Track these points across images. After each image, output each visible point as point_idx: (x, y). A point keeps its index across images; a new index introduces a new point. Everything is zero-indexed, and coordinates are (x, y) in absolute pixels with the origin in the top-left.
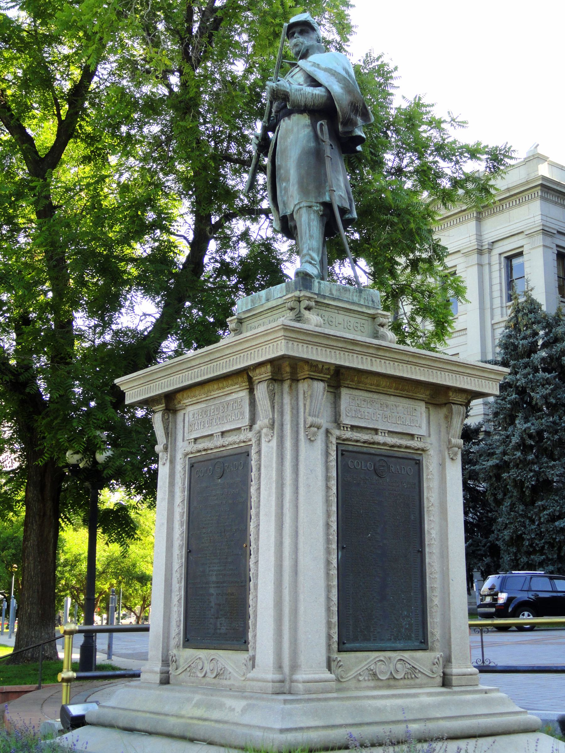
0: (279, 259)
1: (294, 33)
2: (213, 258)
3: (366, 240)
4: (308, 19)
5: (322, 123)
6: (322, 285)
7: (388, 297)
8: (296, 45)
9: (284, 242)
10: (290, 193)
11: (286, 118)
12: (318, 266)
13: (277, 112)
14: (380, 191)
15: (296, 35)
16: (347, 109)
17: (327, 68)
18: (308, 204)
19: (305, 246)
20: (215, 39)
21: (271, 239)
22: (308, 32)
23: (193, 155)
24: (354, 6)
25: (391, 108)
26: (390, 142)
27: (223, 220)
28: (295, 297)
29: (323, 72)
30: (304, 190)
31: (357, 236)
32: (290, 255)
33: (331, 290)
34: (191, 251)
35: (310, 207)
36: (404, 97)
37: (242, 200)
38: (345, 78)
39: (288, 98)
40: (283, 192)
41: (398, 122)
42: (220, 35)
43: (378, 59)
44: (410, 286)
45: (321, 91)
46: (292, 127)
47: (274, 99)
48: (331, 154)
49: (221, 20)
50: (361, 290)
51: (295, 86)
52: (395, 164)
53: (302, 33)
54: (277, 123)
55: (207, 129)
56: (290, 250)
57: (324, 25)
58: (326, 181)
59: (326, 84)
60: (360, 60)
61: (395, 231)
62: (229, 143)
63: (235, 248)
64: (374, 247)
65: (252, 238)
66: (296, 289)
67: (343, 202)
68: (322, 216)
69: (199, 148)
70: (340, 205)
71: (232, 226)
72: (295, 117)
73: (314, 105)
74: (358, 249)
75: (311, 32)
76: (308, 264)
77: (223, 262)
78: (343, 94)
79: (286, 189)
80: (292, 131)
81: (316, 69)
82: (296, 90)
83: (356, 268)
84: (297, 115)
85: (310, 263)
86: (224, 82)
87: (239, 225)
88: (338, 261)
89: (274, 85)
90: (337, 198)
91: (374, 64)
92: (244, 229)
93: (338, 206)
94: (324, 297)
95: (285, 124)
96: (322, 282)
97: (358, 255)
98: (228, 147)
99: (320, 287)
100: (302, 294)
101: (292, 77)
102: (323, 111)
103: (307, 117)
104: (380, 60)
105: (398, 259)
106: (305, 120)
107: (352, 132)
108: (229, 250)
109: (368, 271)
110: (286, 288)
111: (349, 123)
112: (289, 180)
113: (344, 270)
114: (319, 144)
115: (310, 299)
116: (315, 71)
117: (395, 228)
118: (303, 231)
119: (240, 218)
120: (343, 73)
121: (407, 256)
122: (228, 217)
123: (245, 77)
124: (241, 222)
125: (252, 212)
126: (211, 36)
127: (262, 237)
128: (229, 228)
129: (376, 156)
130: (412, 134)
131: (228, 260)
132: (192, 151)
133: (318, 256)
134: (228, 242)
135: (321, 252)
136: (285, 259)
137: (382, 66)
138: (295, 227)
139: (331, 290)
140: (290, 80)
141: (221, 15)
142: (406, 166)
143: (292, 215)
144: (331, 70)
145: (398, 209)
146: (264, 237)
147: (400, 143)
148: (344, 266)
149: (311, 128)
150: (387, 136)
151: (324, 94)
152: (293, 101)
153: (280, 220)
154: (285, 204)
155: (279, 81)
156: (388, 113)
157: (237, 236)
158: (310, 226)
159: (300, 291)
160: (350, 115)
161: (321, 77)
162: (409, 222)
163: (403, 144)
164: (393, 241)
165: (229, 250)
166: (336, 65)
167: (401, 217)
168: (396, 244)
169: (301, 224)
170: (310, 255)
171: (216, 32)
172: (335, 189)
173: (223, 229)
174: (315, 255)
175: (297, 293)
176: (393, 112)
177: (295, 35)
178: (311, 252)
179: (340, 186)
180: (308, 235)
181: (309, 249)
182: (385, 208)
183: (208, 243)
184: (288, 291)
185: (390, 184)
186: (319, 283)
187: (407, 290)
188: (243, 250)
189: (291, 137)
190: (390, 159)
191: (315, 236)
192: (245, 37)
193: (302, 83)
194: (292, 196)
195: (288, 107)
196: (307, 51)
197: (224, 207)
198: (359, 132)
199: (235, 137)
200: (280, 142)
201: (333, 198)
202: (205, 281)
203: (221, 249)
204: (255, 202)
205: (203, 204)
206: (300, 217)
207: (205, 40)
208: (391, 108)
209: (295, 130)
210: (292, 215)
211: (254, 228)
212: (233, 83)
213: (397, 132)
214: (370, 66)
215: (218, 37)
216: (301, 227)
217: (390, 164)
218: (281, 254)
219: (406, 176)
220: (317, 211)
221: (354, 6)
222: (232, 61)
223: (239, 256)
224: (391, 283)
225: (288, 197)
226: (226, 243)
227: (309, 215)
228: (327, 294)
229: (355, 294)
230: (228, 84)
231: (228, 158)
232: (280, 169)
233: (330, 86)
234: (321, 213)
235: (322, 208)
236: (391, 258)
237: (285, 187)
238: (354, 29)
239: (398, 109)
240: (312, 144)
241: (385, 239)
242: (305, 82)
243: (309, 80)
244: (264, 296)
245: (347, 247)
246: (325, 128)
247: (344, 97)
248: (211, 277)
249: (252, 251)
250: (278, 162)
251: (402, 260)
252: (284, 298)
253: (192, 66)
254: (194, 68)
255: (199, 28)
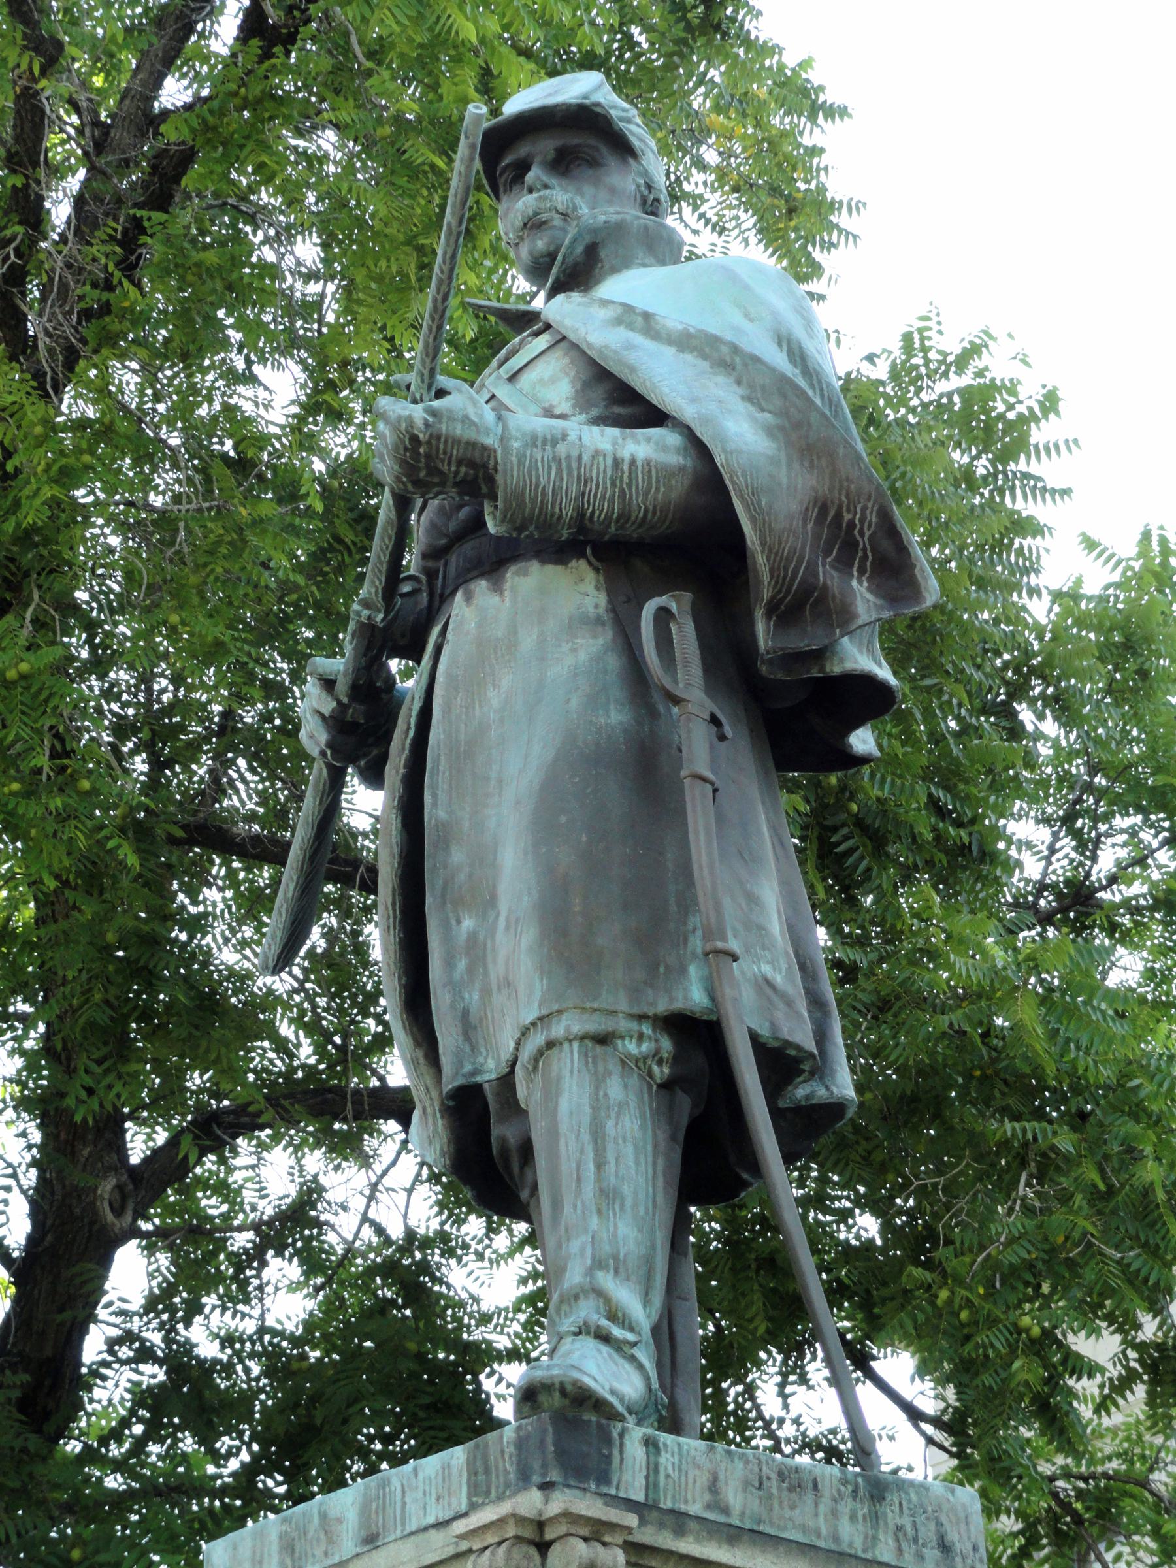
0: (469, 1347)
1: (523, 167)
2: (128, 1337)
3: (916, 1241)
4: (598, 97)
5: (671, 610)
6: (665, 1460)
7: (1032, 1542)
8: (533, 224)
9: (499, 1259)
10: (496, 970)
11: (481, 586)
12: (645, 1356)
13: (433, 554)
14: (984, 995)
15: (533, 175)
16: (800, 537)
17: (695, 319)
18: (594, 1024)
19: (575, 1246)
20: (153, 249)
21: (426, 1243)
22: (594, 163)
23: (31, 810)
24: (843, 112)
25: (1034, 591)
26: (1030, 762)
27: (186, 1142)
28: (520, 1520)
29: (669, 351)
30: (570, 952)
31: (868, 1225)
32: (528, 1326)
33: (713, 1486)
34: (17, 1301)
35: (603, 1039)
36: (1090, 544)
37: (283, 1047)
38: (783, 382)
39: (491, 481)
40: (462, 964)
41: (1069, 657)
42: (176, 229)
43: (961, 363)
44: (1144, 1484)
45: (664, 448)
46: (513, 630)
47: (417, 483)
48: (714, 764)
49: (186, 158)
50: (878, 1489)
51: (526, 421)
52: (1060, 869)
53: (564, 164)
54: (438, 602)
55: (109, 694)
56: (531, 1299)
57: (696, 201)
58: (687, 902)
59: (687, 412)
60: (871, 358)
61: (1065, 1198)
62: (222, 763)
63: (240, 1293)
64: (959, 1281)
65: (331, 1237)
66: (524, 1478)
67: (780, 1015)
68: (666, 1086)
69: (64, 779)
70: (764, 1031)
71: (238, 1177)
72: (528, 581)
73: (624, 517)
74: (878, 1298)
75: (612, 162)
76: (589, 1344)
77: (180, 1361)
78: (773, 461)
79: (477, 950)
80: (512, 645)
81: (638, 339)
82: (534, 441)
83: (866, 1392)
84: (534, 566)
85: (604, 1338)
86: (206, 470)
87: (268, 1172)
88: (773, 1360)
89: (418, 413)
90: (748, 995)
91: (942, 386)
92: (293, 1190)
93: (754, 1038)
94: (679, 1521)
95: (475, 615)
96: (665, 1438)
97: (875, 1326)
98: (218, 786)
99: (653, 1469)
100: (554, 1508)
101: (513, 378)
102: (678, 549)
103: (590, 576)
104: (976, 363)
105: (1080, 1344)
106: (578, 591)
107: (820, 655)
108: (210, 1300)
109: (929, 1406)
110: (473, 1473)
111: (804, 604)
112: (492, 901)
113: (801, 1402)
114: (653, 714)
115: (597, 1531)
116: (629, 346)
117: (1065, 1182)
118: (566, 1167)
119: (276, 1138)
120: (779, 360)
121: (1126, 1325)
122: (215, 1130)
123: (303, 439)
124: (279, 1159)
125: (336, 1108)
126: (130, 239)
127: (380, 1230)
128: (223, 1189)
129: (959, 824)
130: (1137, 718)
131: (208, 1349)
132: (29, 793)
133: (646, 1302)
134: (214, 1254)
135: (660, 1280)
136: (502, 1343)
137: (978, 396)
138: (526, 1150)
139: (713, 1486)
140: (504, 393)
141: (186, 135)
142: (1113, 880)
143: (507, 1081)
144: (714, 341)
145: (1076, 1090)
146: (396, 1232)
147: (1078, 767)
148: (804, 1380)
149: (606, 636)
150: (1015, 731)
151: (674, 459)
152: (518, 496)
153: (446, 1111)
154: (468, 1026)
155: (441, 393)
156: (1014, 616)
157: (256, 1227)
158: (601, 1137)
159: (546, 1487)
160: (812, 569)
161: (664, 376)
162: (1132, 1154)
163: (1093, 770)
164: (1053, 1251)
165: (210, 1300)
166: (738, 319)
167: (1091, 1129)
168: (1071, 1264)
169: (553, 1133)
170: (600, 1293)
171: (158, 216)
172: (734, 945)
173: (187, 1192)
174: (627, 1297)
175: (530, 1502)
176: (1040, 610)
177: (530, 177)
178: (607, 1281)
179: (765, 943)
180: (589, 1188)
181: (599, 1264)
182: (1006, 1081)
183: (105, 1261)
184: (480, 1493)
185: (1033, 964)
186: (650, 1443)
187: (1127, 1504)
188: (286, 1300)
189: (506, 681)
190: (1031, 845)
191: (627, 1190)
192: (308, 250)
193: (564, 407)
194: (508, 980)
195: (492, 527)
196: (592, 251)
197: (195, 1080)
198: (862, 657)
199: (254, 735)
200: (447, 708)
201: (728, 992)
202: (90, 1455)
203: (169, 1291)
204: (353, 1055)
205: (82, 1061)
206: (551, 1094)
207: (101, 253)
208: (1034, 591)
209: (528, 641)
210: (507, 1081)
211: (343, 1184)
212: (242, 465)
213: (1063, 706)
214: (925, 396)
215: (168, 241)
216: (554, 1155)
217: (1033, 869)
218: (485, 1319)
219: (1112, 928)
220: (641, 1061)
221: (843, 112)
222: (240, 365)
223: (262, 1330)
224: (1045, 1468)
225: (486, 992)
226: (202, 1265)
227: (599, 1082)
228: (695, 1509)
229: (846, 1507)
230: (218, 469)
231: (215, 836)
232: (445, 844)
233: (706, 420)
234: (661, 1072)
235: (666, 1045)
236: (1048, 1334)
237: (472, 937)
238: (842, 219)
239: (1067, 597)
240: (617, 716)
241: (1011, 1241)
242: (582, 402)
243: (599, 392)
244: (352, 1517)
245: (814, 1284)
246: (685, 634)
247: (783, 476)
248: (116, 1435)
249: (333, 1306)
250: (434, 811)
251: (1101, 1347)
252: (460, 1527)
253: (39, 375)
254: (47, 388)
255: (79, 202)
